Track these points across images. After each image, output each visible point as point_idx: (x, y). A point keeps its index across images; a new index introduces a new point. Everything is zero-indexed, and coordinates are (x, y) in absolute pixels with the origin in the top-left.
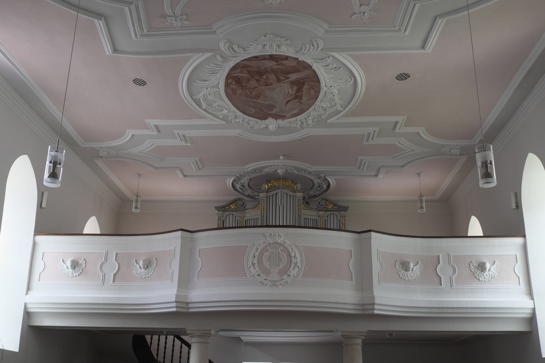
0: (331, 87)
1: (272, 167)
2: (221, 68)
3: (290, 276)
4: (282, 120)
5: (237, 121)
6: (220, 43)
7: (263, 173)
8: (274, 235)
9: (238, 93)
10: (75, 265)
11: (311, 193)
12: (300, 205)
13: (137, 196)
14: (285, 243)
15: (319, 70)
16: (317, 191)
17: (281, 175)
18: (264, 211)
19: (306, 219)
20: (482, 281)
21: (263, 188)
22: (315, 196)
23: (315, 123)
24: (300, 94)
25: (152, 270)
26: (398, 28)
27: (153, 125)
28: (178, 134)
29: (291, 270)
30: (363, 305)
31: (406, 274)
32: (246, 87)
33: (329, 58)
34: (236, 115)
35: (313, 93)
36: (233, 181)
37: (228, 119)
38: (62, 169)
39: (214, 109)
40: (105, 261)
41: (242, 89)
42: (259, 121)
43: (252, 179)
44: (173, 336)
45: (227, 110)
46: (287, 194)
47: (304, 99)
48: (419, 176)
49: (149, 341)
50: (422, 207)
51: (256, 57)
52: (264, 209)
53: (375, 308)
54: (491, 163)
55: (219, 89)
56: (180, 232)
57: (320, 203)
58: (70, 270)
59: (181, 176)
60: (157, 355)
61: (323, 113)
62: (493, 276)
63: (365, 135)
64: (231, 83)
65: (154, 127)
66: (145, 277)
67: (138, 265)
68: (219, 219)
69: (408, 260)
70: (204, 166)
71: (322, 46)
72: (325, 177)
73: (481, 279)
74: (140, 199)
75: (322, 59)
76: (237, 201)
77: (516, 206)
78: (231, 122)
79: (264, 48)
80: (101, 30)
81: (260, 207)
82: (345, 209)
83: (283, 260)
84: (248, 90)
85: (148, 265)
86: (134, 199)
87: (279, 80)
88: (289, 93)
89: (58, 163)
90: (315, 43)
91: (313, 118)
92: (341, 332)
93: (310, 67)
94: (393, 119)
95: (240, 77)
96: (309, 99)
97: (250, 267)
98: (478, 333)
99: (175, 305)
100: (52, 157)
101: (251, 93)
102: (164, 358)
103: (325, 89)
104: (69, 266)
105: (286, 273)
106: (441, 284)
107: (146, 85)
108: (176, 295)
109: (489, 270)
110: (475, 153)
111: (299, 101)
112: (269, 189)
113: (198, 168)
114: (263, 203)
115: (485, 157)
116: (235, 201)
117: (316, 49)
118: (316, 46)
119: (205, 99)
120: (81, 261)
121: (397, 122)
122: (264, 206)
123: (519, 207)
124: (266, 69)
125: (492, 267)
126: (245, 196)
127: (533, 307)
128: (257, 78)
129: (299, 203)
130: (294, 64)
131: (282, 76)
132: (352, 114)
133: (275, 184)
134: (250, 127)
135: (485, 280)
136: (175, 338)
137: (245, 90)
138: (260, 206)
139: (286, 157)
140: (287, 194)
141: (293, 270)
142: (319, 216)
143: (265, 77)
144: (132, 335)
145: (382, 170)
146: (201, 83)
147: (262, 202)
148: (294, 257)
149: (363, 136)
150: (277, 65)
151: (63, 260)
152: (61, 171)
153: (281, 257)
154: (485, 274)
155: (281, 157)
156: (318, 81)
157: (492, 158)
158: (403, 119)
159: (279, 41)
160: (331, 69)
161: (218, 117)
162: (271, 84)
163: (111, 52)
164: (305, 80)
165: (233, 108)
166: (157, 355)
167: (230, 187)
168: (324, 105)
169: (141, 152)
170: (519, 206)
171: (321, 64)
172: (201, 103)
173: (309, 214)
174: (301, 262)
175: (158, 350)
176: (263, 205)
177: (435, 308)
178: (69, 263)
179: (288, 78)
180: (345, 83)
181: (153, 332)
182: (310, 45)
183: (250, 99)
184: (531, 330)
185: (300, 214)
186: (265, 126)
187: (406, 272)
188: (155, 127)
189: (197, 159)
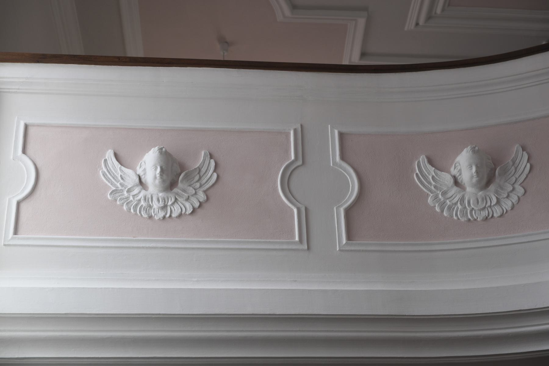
25: (514, 189)
40: (300, 162)
66: (486, 219)
151: (116, 155)
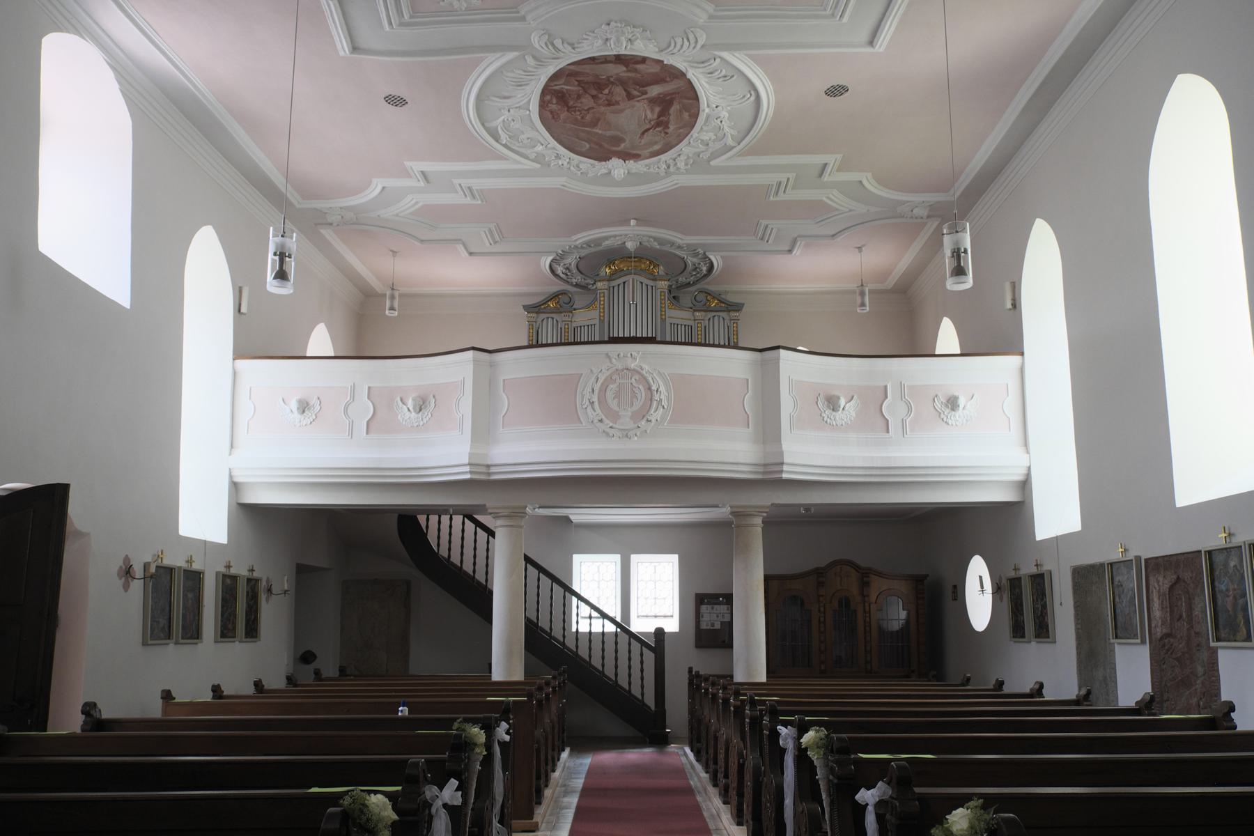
0: (717, 107)
1: (617, 238)
2: (533, 77)
3: (650, 421)
4: (635, 161)
5: (558, 164)
6: (533, 35)
10: (304, 407)
11: (682, 279)
12: (663, 302)
13: (393, 289)
14: (642, 369)
15: (697, 79)
16: (692, 276)
17: (633, 250)
18: (604, 312)
19: (674, 324)
20: (952, 425)
21: (602, 274)
22: (688, 284)
23: (689, 166)
24: (666, 119)
26: (831, 13)
27: (418, 172)
28: (460, 185)
29: (652, 412)
32: (576, 107)
33: (715, 59)
34: (557, 154)
35: (688, 117)
36: (552, 261)
37: (545, 159)
38: (293, 264)
41: (568, 111)
42: (596, 163)
43: (584, 257)
44: (462, 516)
45: (542, 145)
46: (642, 283)
47: (672, 127)
48: (860, 251)
49: (424, 526)
50: (863, 305)
51: (593, 59)
52: (604, 308)
53: (784, 469)
54: (966, 251)
56: (472, 352)
57: (697, 298)
58: (296, 415)
60: (438, 545)
61: (704, 150)
63: (772, 185)
64: (550, 102)
67: (405, 407)
68: (531, 326)
69: (837, 393)
71: (704, 41)
72: (704, 253)
74: (397, 294)
75: (703, 63)
77: (1012, 305)
78: (549, 165)
79: (605, 43)
81: (598, 306)
82: (738, 307)
83: (639, 398)
84: (578, 113)
85: (420, 407)
86: (388, 293)
87: (630, 97)
88: (646, 117)
89: (287, 255)
90: (691, 37)
91: (686, 158)
92: (731, 507)
93: (683, 75)
94: (819, 159)
95: (565, 91)
96: (680, 128)
97: (586, 408)
98: (937, 506)
99: (468, 470)
100: (277, 245)
101: (582, 118)
102: (449, 549)
103: (707, 110)
105: (644, 416)
106: (888, 432)
107: (406, 105)
108: (469, 453)
110: (943, 234)
112: (612, 274)
114: (602, 299)
115: (957, 243)
116: (556, 296)
117: (692, 46)
118: (692, 41)
119: (506, 126)
120: (313, 401)
121: (826, 164)
122: (604, 304)
123: (1017, 306)
124: (608, 77)
125: (969, 404)
126: (572, 285)
127: (1029, 465)
128: (594, 92)
129: (663, 297)
130: (655, 69)
132: (752, 151)
133: (622, 266)
134: (581, 173)
136: (465, 519)
137: (573, 113)
138: (597, 303)
139: (641, 221)
140: (642, 283)
141: (655, 412)
142: (695, 320)
143: (606, 91)
144: (396, 516)
145: (799, 243)
146: (499, 102)
147: (600, 297)
148: (657, 391)
149: (769, 187)
150: (628, 71)
152: (291, 266)
154: (957, 415)
155: (633, 222)
156: (696, 98)
157: (967, 243)
158: (836, 160)
159: (632, 32)
160: (719, 78)
161: (527, 158)
162: (617, 103)
163: (347, 52)
164: (674, 96)
165: (554, 143)
166: (438, 545)
168: (705, 137)
169: (397, 215)
170: (1016, 305)
171: (701, 70)
172: (499, 134)
173: (679, 316)
174: (668, 400)
175: (439, 537)
176: (602, 303)
177: (877, 468)
179: (646, 93)
180: (741, 101)
181: (429, 511)
182: (683, 39)
183: (582, 127)
184: (1022, 500)
185: (664, 317)
186: (606, 171)
187: (834, 413)
188: (421, 175)
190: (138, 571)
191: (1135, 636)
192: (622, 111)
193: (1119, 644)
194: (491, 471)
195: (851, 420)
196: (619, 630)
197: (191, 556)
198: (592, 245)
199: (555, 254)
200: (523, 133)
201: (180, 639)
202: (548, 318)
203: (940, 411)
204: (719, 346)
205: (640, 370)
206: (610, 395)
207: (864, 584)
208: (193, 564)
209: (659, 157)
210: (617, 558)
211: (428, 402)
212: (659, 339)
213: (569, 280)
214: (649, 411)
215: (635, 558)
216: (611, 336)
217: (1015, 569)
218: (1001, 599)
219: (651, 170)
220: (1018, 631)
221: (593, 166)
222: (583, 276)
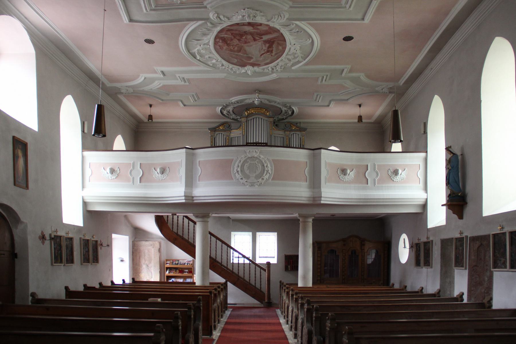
0: (294, 44)
3: (264, 179)
4: (258, 67)
6: (210, 14)
7: (243, 103)
8: (252, 151)
9: (224, 48)
10: (112, 171)
11: (280, 117)
14: (260, 157)
16: (284, 116)
20: (395, 181)
22: (283, 119)
28: (179, 77)
29: (264, 175)
30: (314, 198)
31: (344, 177)
32: (230, 44)
33: (293, 24)
35: (281, 49)
36: (221, 109)
39: (206, 60)
40: (133, 169)
41: (227, 45)
42: (240, 68)
51: (238, 24)
55: (210, 46)
56: (185, 149)
57: (287, 126)
58: (110, 175)
59: (182, 105)
62: (403, 178)
64: (219, 42)
65: (161, 73)
66: (162, 180)
67: (156, 172)
69: (345, 167)
70: (199, 99)
72: (290, 106)
73: (395, 180)
76: (224, 124)
80: (121, 7)
83: (259, 169)
84: (232, 46)
85: (163, 171)
87: (255, 40)
90: (282, 15)
94: (342, 67)
95: (225, 37)
97: (235, 173)
101: (233, 48)
102: (178, 229)
104: (109, 172)
105: (261, 177)
108: (184, 192)
109: (401, 174)
111: (270, 54)
113: (194, 100)
118: (283, 17)
120: (116, 169)
125: (403, 172)
126: (230, 119)
127: (426, 198)
130: (266, 28)
131: (257, 37)
133: (252, 111)
135: (398, 181)
137: (229, 46)
141: (266, 175)
143: (244, 38)
146: (196, 42)
148: (267, 166)
150: (254, 29)
151: (104, 168)
153: (257, 167)
154: (398, 177)
156: (285, 40)
162: (249, 42)
164: (275, 40)
165: (220, 59)
167: (218, 111)
172: (196, 55)
174: (272, 170)
178: (108, 170)
179: (262, 38)
182: (278, 16)
186: (245, 71)
187: (345, 176)
189: (194, 94)
190: (48, 237)
191: (462, 266)
192: (251, 46)
193: (456, 269)
194: (194, 199)
195: (352, 179)
196: (251, 263)
197: (57, 229)
198: (239, 102)
199: (223, 106)
200: (206, 55)
201: (54, 263)
202: (219, 133)
203: (391, 176)
204: (296, 148)
205: (259, 157)
206: (245, 167)
207: (362, 245)
208: (57, 232)
209: (268, 65)
210: (251, 233)
211: (166, 170)
212: (269, 144)
213: (229, 117)
214: (263, 174)
215: (258, 234)
216: (248, 142)
217: (418, 240)
218: (412, 250)
219: (265, 71)
220: (418, 264)
221: (239, 69)
222: (236, 115)
